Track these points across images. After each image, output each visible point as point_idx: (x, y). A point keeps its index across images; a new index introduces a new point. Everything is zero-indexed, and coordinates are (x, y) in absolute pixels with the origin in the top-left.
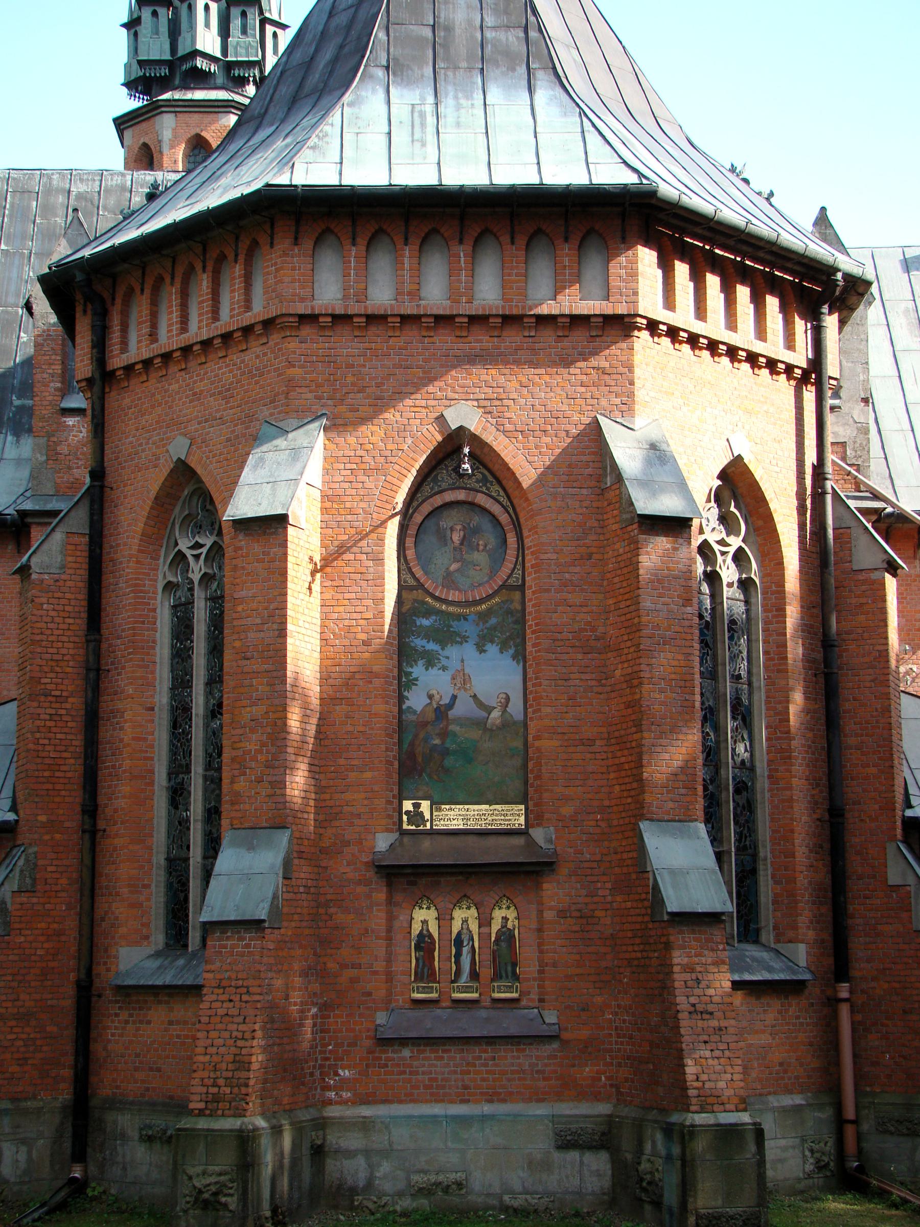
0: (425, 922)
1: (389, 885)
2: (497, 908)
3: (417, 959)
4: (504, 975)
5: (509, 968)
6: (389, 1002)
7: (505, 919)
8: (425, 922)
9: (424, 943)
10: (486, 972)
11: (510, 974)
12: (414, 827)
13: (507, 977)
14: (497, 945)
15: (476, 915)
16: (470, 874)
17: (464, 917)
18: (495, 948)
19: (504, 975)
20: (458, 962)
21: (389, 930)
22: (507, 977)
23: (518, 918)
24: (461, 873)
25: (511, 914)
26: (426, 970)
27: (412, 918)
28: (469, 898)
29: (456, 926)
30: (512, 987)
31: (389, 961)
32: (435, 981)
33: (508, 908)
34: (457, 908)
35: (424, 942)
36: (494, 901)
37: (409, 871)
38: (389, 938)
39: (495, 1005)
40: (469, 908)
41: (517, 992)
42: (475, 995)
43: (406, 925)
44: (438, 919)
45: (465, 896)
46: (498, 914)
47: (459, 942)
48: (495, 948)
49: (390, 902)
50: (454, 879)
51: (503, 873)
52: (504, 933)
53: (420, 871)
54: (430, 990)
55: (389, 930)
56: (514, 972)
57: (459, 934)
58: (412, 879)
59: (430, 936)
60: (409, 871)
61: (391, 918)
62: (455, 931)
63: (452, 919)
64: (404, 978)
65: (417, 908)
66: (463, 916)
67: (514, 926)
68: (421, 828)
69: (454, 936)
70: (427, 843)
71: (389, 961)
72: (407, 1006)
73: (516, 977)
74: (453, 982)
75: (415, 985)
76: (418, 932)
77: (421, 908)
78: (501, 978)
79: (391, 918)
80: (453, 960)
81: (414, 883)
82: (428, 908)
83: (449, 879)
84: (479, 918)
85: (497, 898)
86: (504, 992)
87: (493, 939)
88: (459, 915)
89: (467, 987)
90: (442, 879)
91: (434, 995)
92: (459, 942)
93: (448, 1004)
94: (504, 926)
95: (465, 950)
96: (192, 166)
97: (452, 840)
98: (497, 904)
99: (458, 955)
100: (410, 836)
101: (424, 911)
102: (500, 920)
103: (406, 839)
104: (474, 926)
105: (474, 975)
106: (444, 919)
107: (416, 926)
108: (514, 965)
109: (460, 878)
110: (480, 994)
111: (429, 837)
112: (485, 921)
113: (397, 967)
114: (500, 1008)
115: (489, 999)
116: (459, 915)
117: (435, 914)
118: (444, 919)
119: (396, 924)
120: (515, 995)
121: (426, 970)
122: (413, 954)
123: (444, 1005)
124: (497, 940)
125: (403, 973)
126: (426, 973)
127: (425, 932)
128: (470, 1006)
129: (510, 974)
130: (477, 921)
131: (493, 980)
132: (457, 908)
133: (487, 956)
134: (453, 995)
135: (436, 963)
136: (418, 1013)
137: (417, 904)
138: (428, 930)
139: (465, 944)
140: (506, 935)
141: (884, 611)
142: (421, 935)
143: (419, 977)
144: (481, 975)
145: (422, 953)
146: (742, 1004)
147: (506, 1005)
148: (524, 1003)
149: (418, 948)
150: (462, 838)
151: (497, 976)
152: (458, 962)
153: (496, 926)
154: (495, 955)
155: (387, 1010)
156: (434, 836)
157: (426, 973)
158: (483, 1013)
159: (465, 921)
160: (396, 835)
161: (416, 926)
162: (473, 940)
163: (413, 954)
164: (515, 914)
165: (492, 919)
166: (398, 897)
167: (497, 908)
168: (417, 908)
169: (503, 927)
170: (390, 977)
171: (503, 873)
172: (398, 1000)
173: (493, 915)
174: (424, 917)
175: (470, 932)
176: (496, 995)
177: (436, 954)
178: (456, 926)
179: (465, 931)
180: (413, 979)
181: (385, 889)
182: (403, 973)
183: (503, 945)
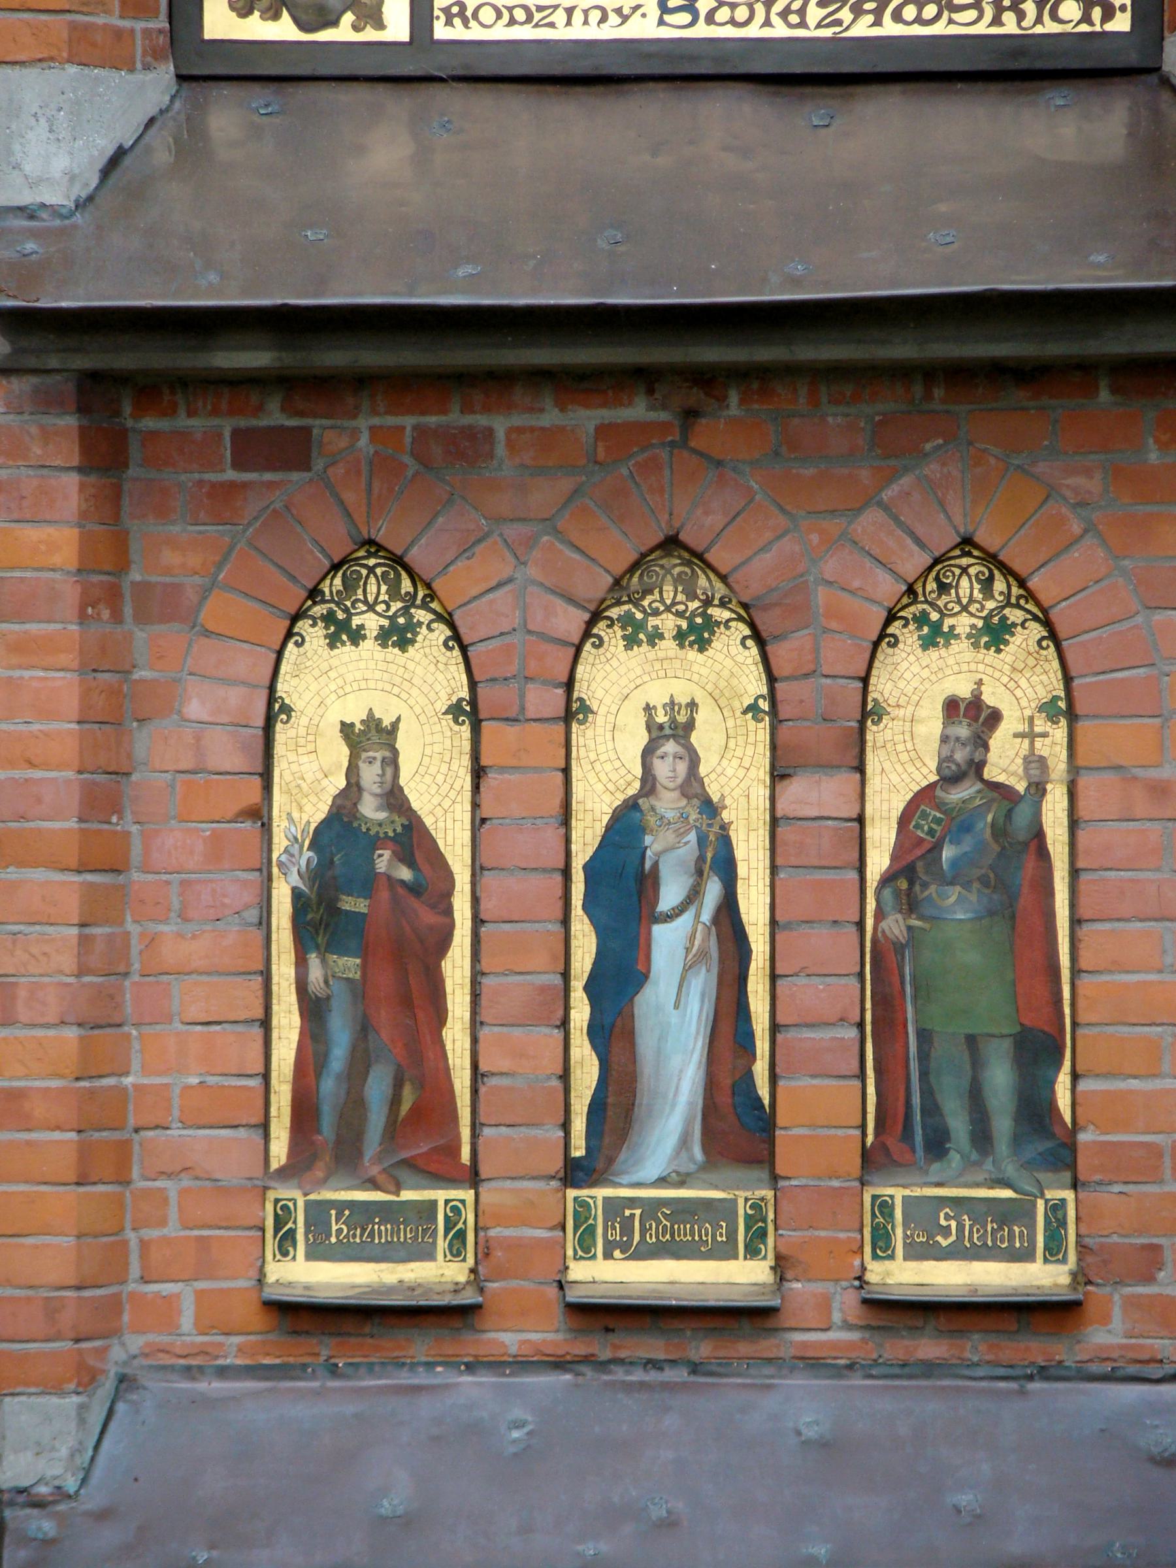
0: (371, 738)
1: (104, 456)
2: (909, 637)
3: (313, 1009)
4: (958, 1125)
5: (1000, 1078)
6: (105, 1321)
7: (973, 716)
8: (371, 738)
9: (368, 898)
10: (824, 1107)
11: (1003, 1125)
12: (284, 29)
13: (982, 1138)
14: (911, 905)
15: (754, 685)
16: (708, 379)
17: (665, 701)
18: (895, 926)
19: (958, 1125)
20: (614, 1033)
21: (105, 791)
22: (982, 1138)
23: (1067, 709)
24: (645, 378)
25: (1019, 681)
26: (377, 1088)
27: (274, 711)
28: (698, 558)
29: (606, 768)
30: (1011, 1215)
31: (100, 1019)
32: (442, 1167)
33: (995, 634)
34: (613, 638)
35: (368, 883)
36: (888, 589)
37: (255, 358)
38: (103, 858)
39: (896, 1348)
40: (697, 635)
41: (1054, 1251)
42: (742, 1276)
43: (228, 753)
44: (470, 712)
45: (671, 543)
46: (917, 683)
47: (623, 885)
48: (895, 926)
49: (107, 581)
50: (586, 419)
51: (959, 376)
52: (959, 823)
53: (334, 357)
54: (411, 1233)
55: (105, 791)
56: (1035, 1112)
57: (626, 824)
58: (274, 416)
59: (413, 839)
60: (255, 358)
61: (115, 709)
62: (595, 803)
63: (572, 712)
64: (222, 1151)
65: (314, 634)
66: (658, 694)
67: (1036, 764)
68: (344, 32)
69: (586, 839)
70: (383, 152)
71: (100, 1019)
72: (233, 1349)
73: (1049, 1142)
74: (576, 1173)
75: (294, 1195)
76: (317, 811)
77: (342, 632)
78: (937, 1146)
79: (115, 709)
80: (581, 1013)
81: (291, 452)
82: (398, 636)
83: (551, 417)
84: (773, 708)
85: (913, 562)
86: (957, 1253)
87: (878, 862)
88: (625, 684)
89: (684, 1210)
90: (500, 425)
91: (439, 1274)
92: (623, 885)
93: (549, 1334)
94: (965, 766)
95: (669, 943)
96: (195, 1332)
97: (576, 124)
98: (910, 608)
99: (619, 979)
100: (259, 95)
101: (366, 658)
102: (932, 725)
103: (226, 117)
104: (735, 767)
105: (739, 1127)
106: (517, 710)
107: (309, 767)
108: (1039, 1050)
109: (637, 410)
110: (781, 1266)
111: (398, 105)
112: (818, 736)
113: (164, 1066)
114: (929, 1369)
115: (845, 1304)
116: (625, 684)
117: (449, 679)
118: (517, 710)
119: (158, 751)
120: (1042, 1276)
121: (377, 1088)
122: (284, 971)
123: (509, 1340)
124: (907, 872)
125: (209, 1111)
126: (379, 1109)
127: (370, 809)
128: (703, 1349)
129: (1003, 1125)
130: (761, 732)
131: (873, 1161)
132: (613, 638)
133: (835, 991)
134: (579, 1271)
135: (456, 1037)
136: (316, 1405)
137: (311, 603)
138: (395, 799)
139: (670, 895)
140: (977, 838)
141: (872, 985)
142: (339, 827)
143: (325, 1136)
144: (790, 1132)
145: (349, 965)
146: (39, 1529)
147: (975, 1347)
148: (1107, 1334)
149: (318, 922)
150: (648, 110)
151: (904, 1134)
152: (614, 1033)
153: (901, 766)
154: (888, 977)
155: (87, 1378)
156: (440, 95)
157: (379, 1109)
158: (803, 1408)
159: (671, 730)
160: (156, 86)
161: (309, 767)
162: (727, 869)
163: (284, 971)
164: (1045, 680)
165: (868, 713)
166: (174, 549)
167: (909, 637)
168: (314, 634)
169: (950, 777)
170: (106, 1143)
171: (959, 376)
172: (170, 1303)
173: (882, 686)
174: (366, 700)
175: (710, 808)
176: (902, 1275)
177: (456, 968)
178: (606, 768)
179: (668, 803)
180: (279, 1149)
181: (69, 488)
182: (209, 1111)
183: (957, 906)
